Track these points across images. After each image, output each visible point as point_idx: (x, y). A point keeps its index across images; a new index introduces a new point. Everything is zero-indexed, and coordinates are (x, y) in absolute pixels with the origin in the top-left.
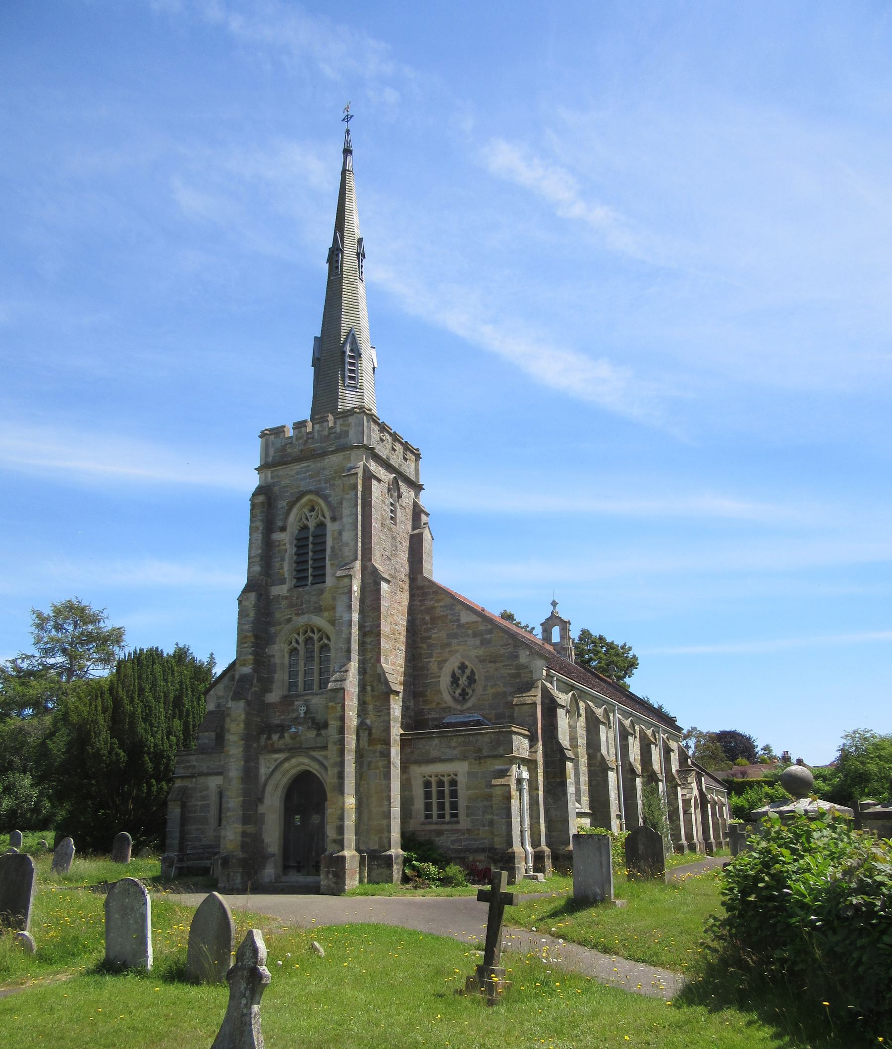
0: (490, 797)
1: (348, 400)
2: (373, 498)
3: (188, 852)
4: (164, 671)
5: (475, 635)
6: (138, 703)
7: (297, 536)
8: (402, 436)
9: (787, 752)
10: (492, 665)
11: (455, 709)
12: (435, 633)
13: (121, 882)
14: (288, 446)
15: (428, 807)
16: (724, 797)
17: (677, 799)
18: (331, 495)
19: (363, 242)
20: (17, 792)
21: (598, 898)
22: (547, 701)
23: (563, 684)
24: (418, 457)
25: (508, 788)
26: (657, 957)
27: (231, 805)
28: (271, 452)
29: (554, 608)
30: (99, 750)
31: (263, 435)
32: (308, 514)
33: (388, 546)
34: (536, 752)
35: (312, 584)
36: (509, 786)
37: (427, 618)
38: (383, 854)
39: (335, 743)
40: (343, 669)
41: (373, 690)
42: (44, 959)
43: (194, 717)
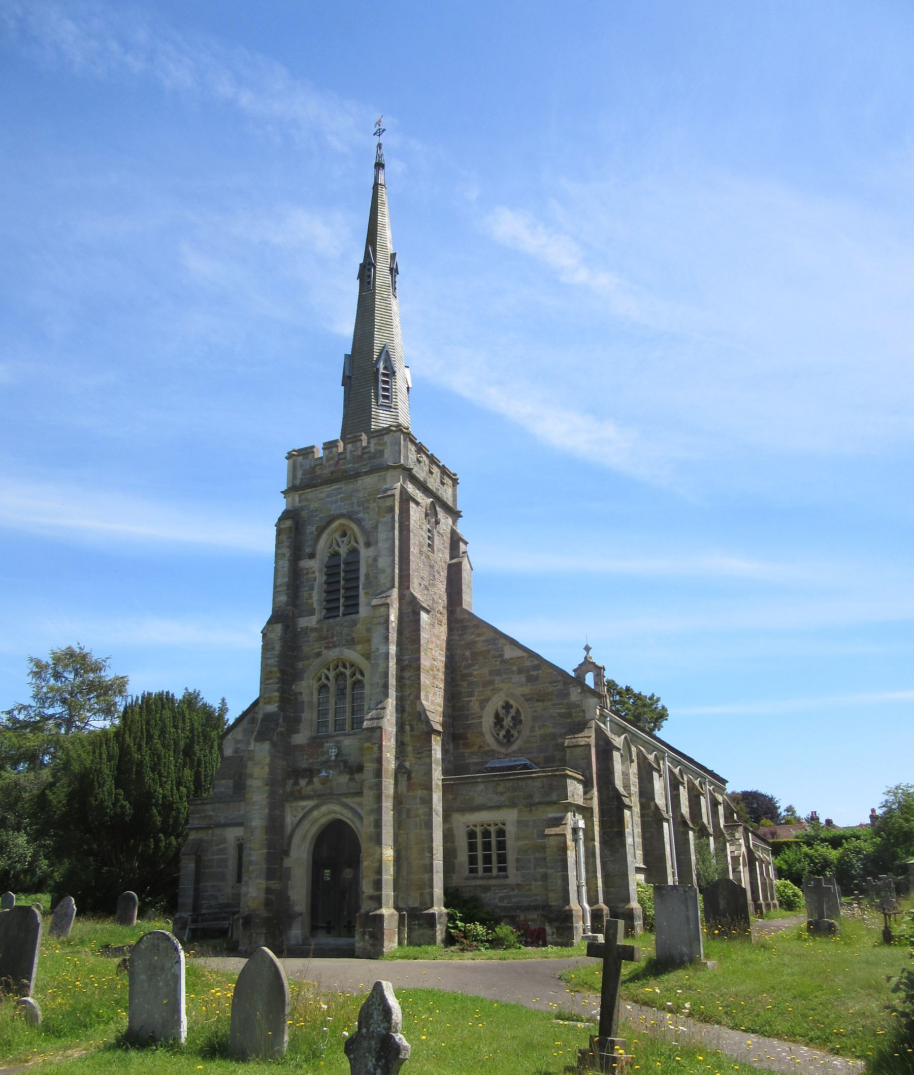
0: (544, 848)
1: (381, 419)
2: (412, 522)
3: (204, 911)
4: (174, 717)
5: (520, 671)
6: (146, 751)
7: (327, 562)
8: (439, 459)
9: (815, 812)
11: (499, 753)
12: (475, 670)
13: (149, 936)
14: (317, 468)
15: (473, 860)
16: (768, 856)
17: (726, 856)
18: (364, 518)
19: (397, 257)
20: (10, 852)
21: (686, 958)
22: (601, 743)
24: (455, 482)
25: (563, 838)
26: (770, 1026)
27: (254, 858)
28: (299, 474)
29: (588, 654)
30: (102, 802)
31: (290, 456)
32: (339, 540)
33: (426, 574)
34: (591, 799)
35: (344, 615)
36: (564, 835)
37: (468, 653)
38: (425, 912)
39: (371, 788)
40: (379, 706)
41: (412, 730)
42: (51, 1031)
43: (206, 767)
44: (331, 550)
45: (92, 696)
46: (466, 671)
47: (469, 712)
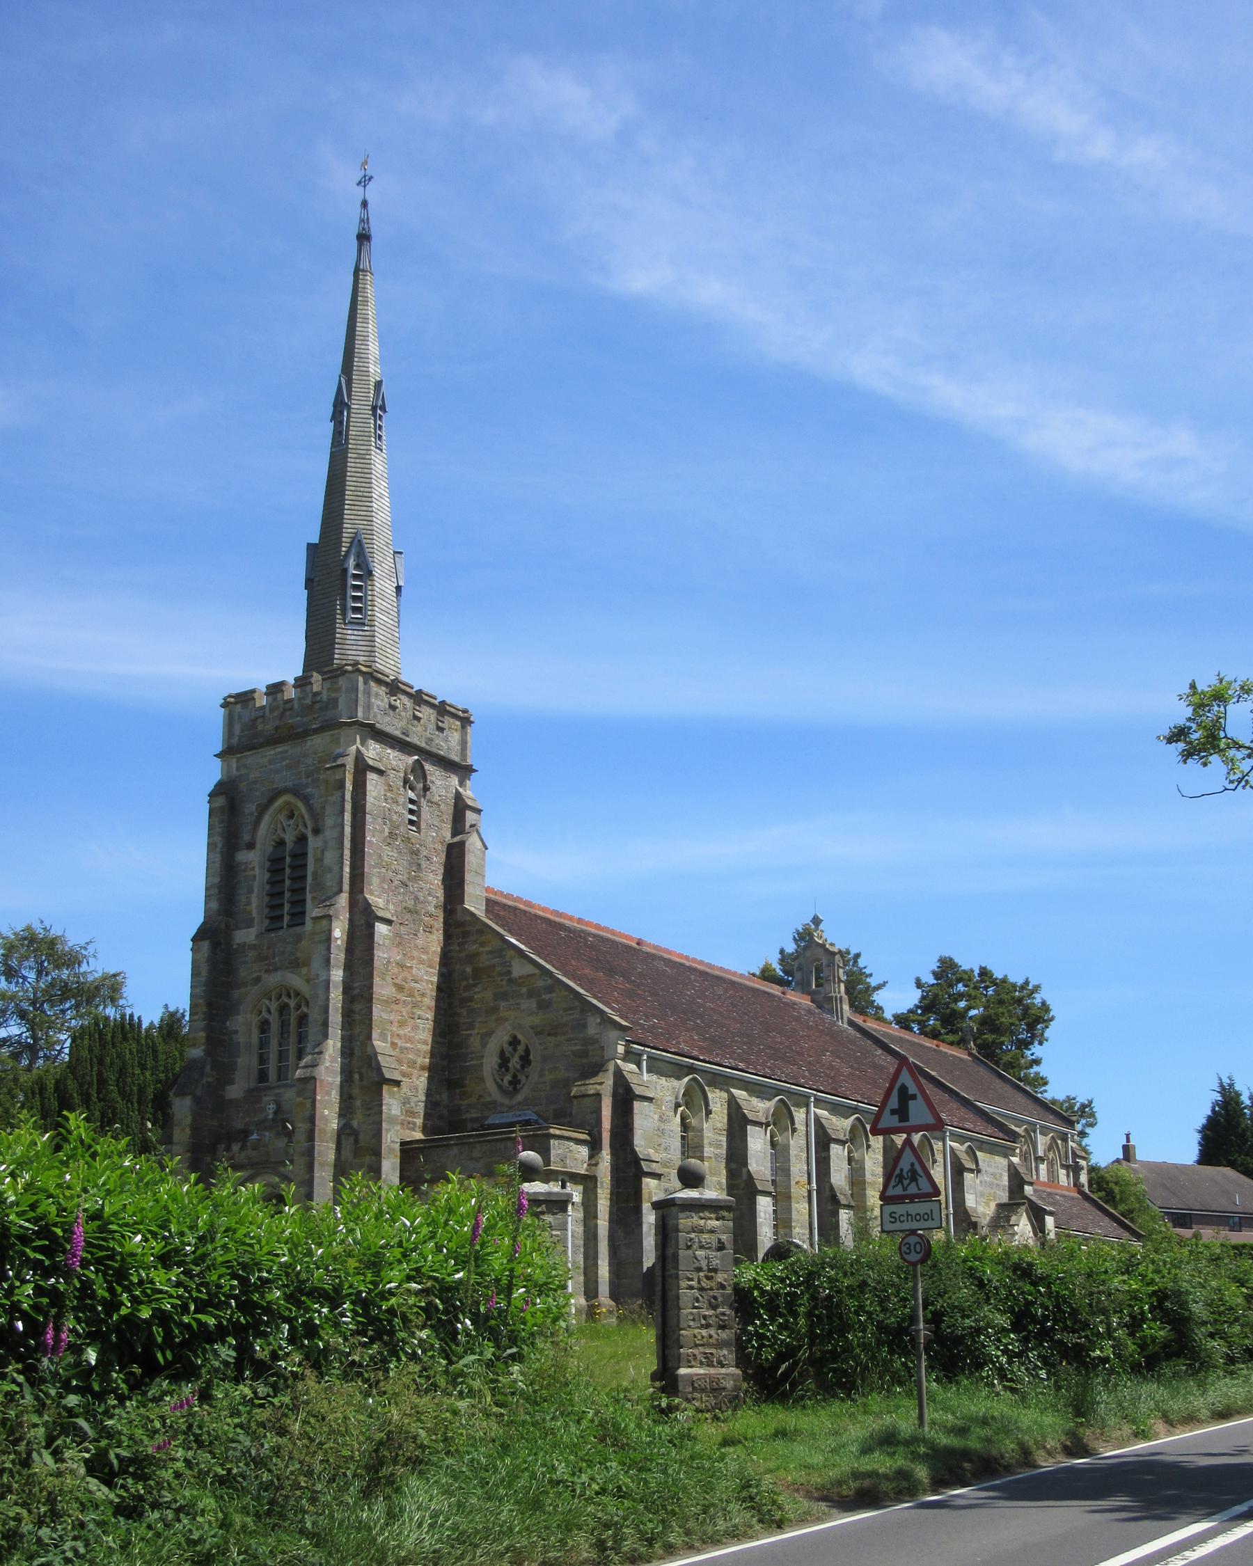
5: (531, 995)
10: (549, 1038)
11: (502, 1105)
14: (259, 721)
22: (621, 1091)
23: (667, 1064)
28: (237, 729)
35: (290, 926)
37: (469, 970)
40: (317, 1050)
41: (361, 1079)
44: (274, 837)
45: (67, 1005)
46: (466, 994)
47: (469, 1050)
